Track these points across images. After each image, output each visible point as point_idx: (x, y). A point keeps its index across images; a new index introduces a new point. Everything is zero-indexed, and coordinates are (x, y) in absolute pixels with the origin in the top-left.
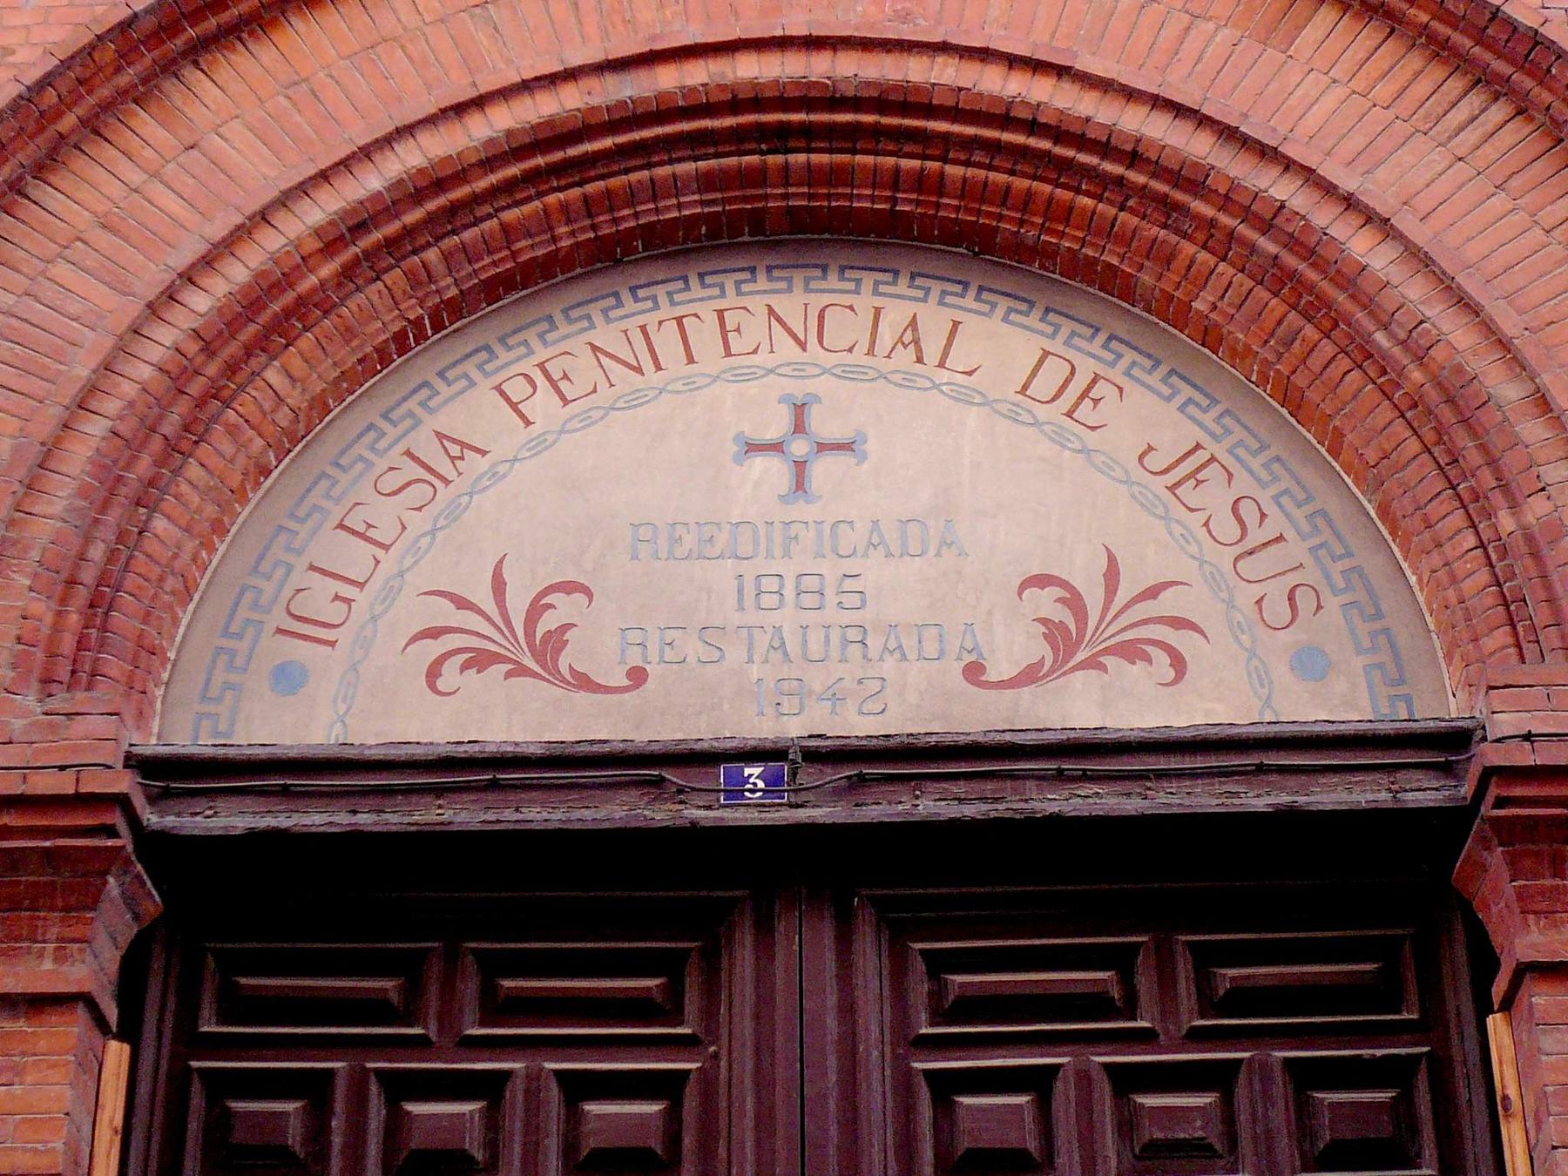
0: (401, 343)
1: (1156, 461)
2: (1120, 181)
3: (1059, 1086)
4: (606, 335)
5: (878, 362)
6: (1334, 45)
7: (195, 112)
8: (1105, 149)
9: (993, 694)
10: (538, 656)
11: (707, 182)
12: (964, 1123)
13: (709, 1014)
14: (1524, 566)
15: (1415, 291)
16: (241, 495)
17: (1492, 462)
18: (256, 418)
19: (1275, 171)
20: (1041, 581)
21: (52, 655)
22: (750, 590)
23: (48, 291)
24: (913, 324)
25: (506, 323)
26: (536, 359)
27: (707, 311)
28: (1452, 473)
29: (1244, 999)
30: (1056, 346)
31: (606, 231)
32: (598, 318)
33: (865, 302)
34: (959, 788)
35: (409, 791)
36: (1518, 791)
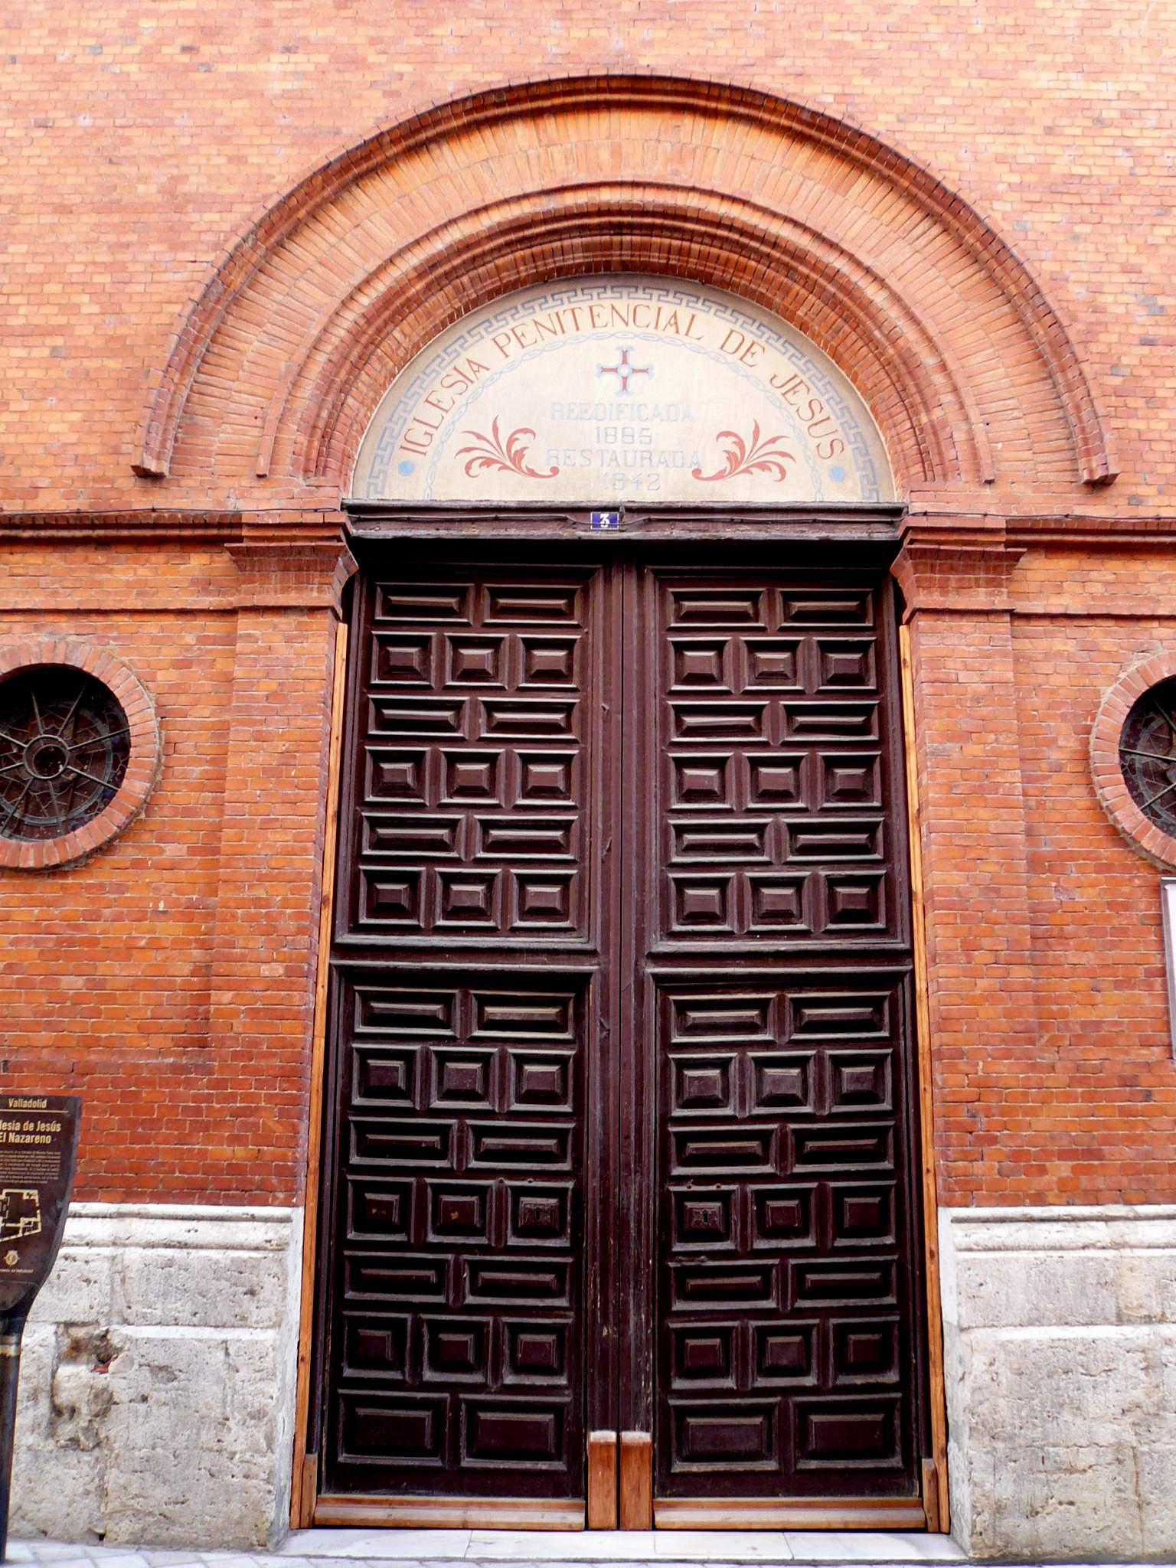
0: (451, 319)
1: (778, 382)
2: (768, 255)
3: (726, 648)
4: (541, 316)
5: (659, 332)
6: (866, 195)
7: (357, 208)
8: (762, 240)
9: (705, 483)
10: (513, 461)
11: (586, 248)
12: (687, 662)
13: (585, 614)
14: (930, 438)
15: (893, 313)
16: (383, 387)
17: (920, 392)
18: (389, 352)
19: (836, 254)
20: (727, 434)
21: (308, 460)
22: (602, 435)
23: (298, 294)
24: (675, 315)
25: (497, 309)
26: (510, 327)
27: (585, 306)
28: (903, 395)
29: (802, 616)
30: (737, 328)
31: (541, 269)
32: (537, 308)
33: (654, 304)
34: (690, 525)
35: (461, 521)
36: (920, 537)
